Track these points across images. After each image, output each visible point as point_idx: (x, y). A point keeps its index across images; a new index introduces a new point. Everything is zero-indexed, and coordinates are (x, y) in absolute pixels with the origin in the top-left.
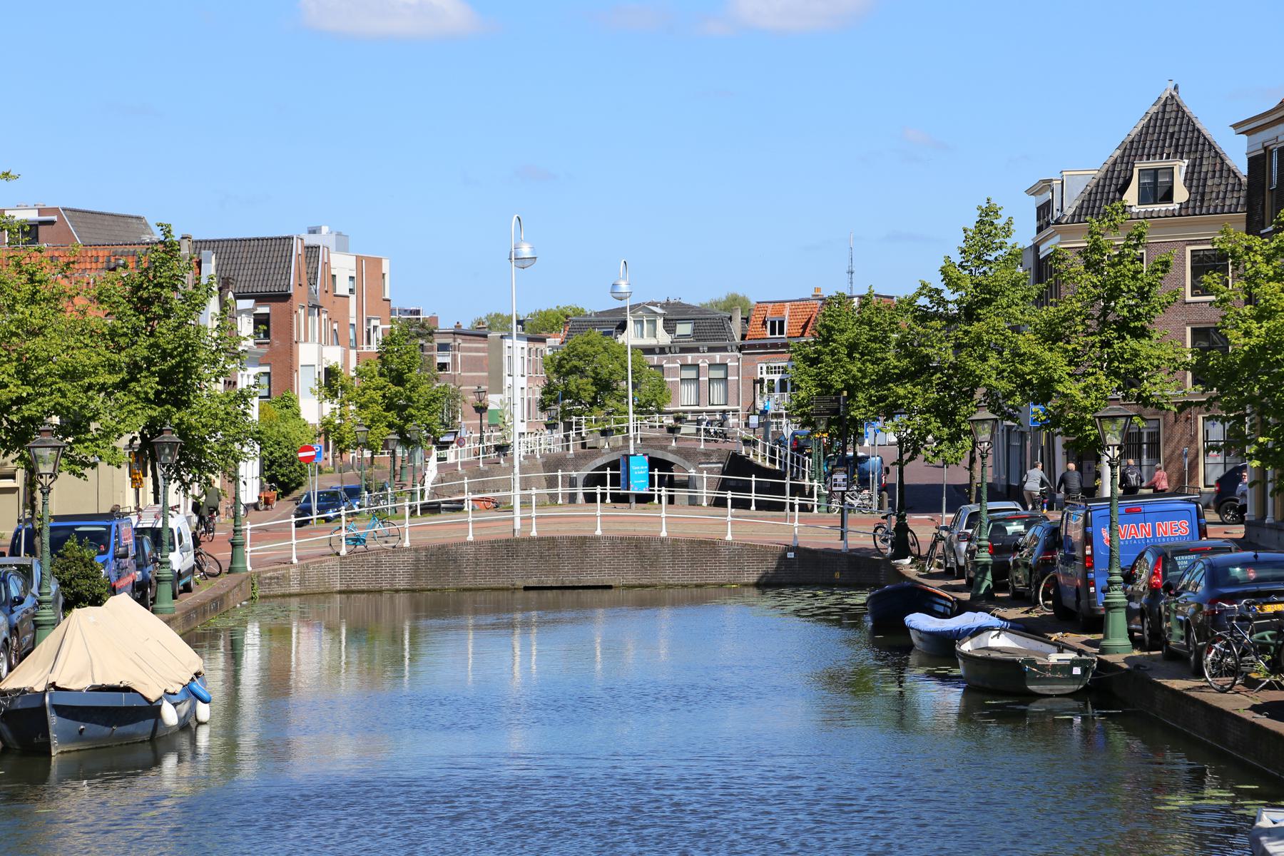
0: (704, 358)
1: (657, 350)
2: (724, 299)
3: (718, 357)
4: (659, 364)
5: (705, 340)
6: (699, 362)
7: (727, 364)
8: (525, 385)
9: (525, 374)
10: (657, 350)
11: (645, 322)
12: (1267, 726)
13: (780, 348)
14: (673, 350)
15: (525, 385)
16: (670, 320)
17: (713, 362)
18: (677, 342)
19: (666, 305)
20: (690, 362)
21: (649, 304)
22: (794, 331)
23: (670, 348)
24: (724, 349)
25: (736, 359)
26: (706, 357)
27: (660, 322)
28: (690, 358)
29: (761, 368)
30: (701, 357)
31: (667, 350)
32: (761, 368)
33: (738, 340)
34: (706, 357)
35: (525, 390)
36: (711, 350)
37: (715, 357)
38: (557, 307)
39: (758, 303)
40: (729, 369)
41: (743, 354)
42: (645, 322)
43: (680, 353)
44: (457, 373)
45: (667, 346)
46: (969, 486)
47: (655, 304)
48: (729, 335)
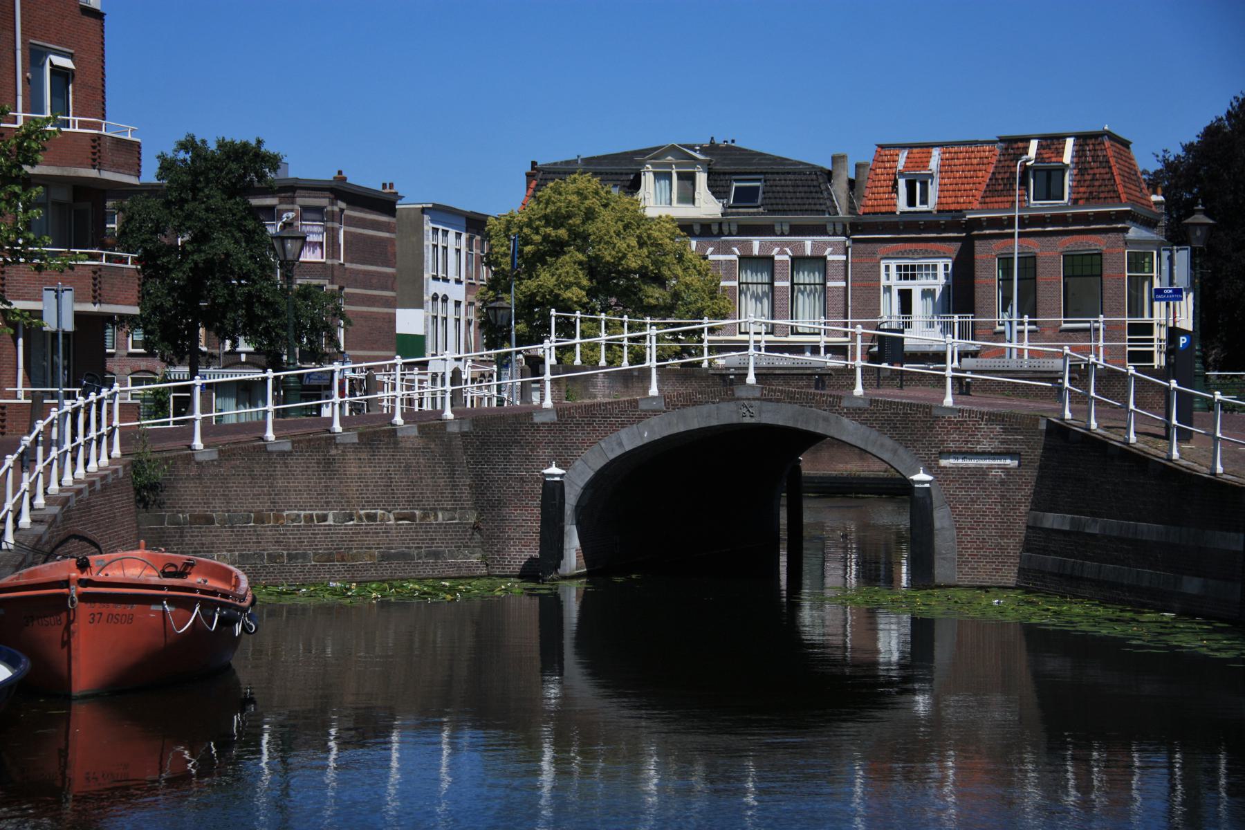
0: (782, 245)
1: (697, 229)
2: (1202, 131)
3: (808, 245)
4: (764, 254)
5: (784, 212)
6: (774, 253)
7: (772, 258)
8: (461, 297)
9: (463, 278)
10: (697, 229)
11: (675, 177)
12: (564, 616)
13: (945, 231)
14: (725, 229)
15: (461, 297)
16: (719, 174)
17: (799, 254)
18: (732, 214)
19: (711, 149)
20: (808, 252)
21: (685, 146)
22: (950, 200)
23: (720, 224)
24: (819, 230)
25: (842, 250)
26: (788, 244)
27: (702, 178)
28: (756, 245)
29: (887, 268)
30: (776, 244)
31: (715, 229)
32: (887, 268)
33: (842, 213)
34: (788, 244)
35: (463, 306)
36: (797, 230)
37: (802, 245)
38: (1198, 136)
39: (882, 147)
40: (777, 266)
41: (855, 241)
42: (675, 177)
43: (789, 235)
44: (336, 262)
45: (713, 221)
46: (57, 331)
47: (692, 148)
48: (828, 203)
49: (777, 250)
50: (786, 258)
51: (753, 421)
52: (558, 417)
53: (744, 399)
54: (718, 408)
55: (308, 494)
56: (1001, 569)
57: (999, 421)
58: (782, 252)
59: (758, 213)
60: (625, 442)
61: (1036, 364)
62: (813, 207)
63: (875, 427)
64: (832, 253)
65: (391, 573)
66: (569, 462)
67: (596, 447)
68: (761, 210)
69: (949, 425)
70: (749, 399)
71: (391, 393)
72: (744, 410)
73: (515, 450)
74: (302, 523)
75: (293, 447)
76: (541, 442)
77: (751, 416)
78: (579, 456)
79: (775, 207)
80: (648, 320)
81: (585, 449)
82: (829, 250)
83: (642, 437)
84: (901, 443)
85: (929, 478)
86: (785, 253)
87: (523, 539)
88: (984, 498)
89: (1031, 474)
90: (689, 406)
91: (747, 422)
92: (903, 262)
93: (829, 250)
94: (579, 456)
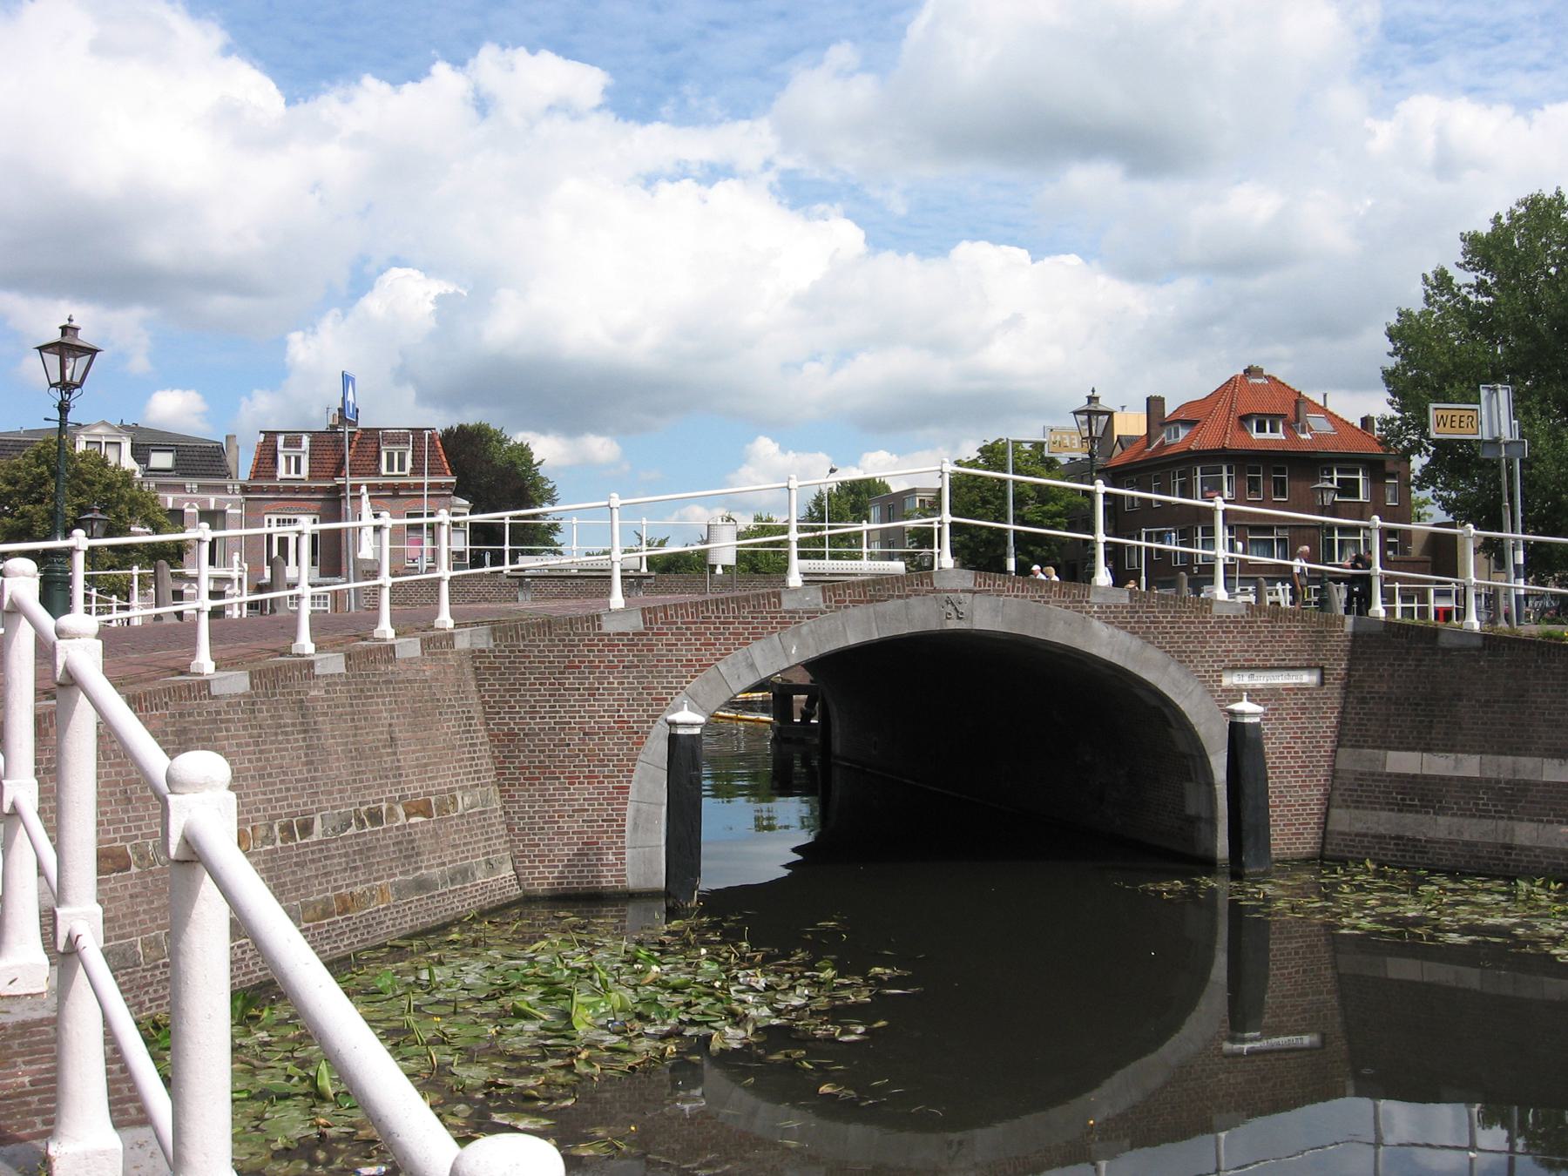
0: (191, 501)
7: (183, 511)
17: (205, 508)
24: (223, 489)
29: (270, 521)
32: (270, 521)
34: (195, 500)
37: (207, 502)
41: (247, 499)
49: (187, 504)
50: (195, 511)
51: (963, 625)
52: (645, 623)
53: (947, 591)
54: (907, 606)
55: (282, 782)
56: (1303, 834)
57: (1298, 621)
58: (191, 506)
59: (172, 476)
60: (758, 662)
61: (849, 567)
62: (216, 472)
63: (1137, 633)
64: (231, 508)
65: (412, 920)
66: (665, 699)
67: (711, 671)
68: (174, 473)
69: (1235, 627)
70: (956, 591)
71: (115, 606)
72: (949, 608)
73: (570, 680)
74: (279, 844)
75: (252, 686)
76: (617, 667)
77: (959, 618)
78: (682, 688)
79: (186, 471)
80: (1499, 386)
81: (692, 677)
82: (229, 505)
83: (787, 656)
84: (1173, 656)
85: (1260, 709)
86: (193, 507)
87: (586, 832)
88: (1280, 733)
89: (1335, 692)
90: (862, 602)
91: (952, 627)
92: (282, 517)
93: (229, 505)
94: (682, 688)
